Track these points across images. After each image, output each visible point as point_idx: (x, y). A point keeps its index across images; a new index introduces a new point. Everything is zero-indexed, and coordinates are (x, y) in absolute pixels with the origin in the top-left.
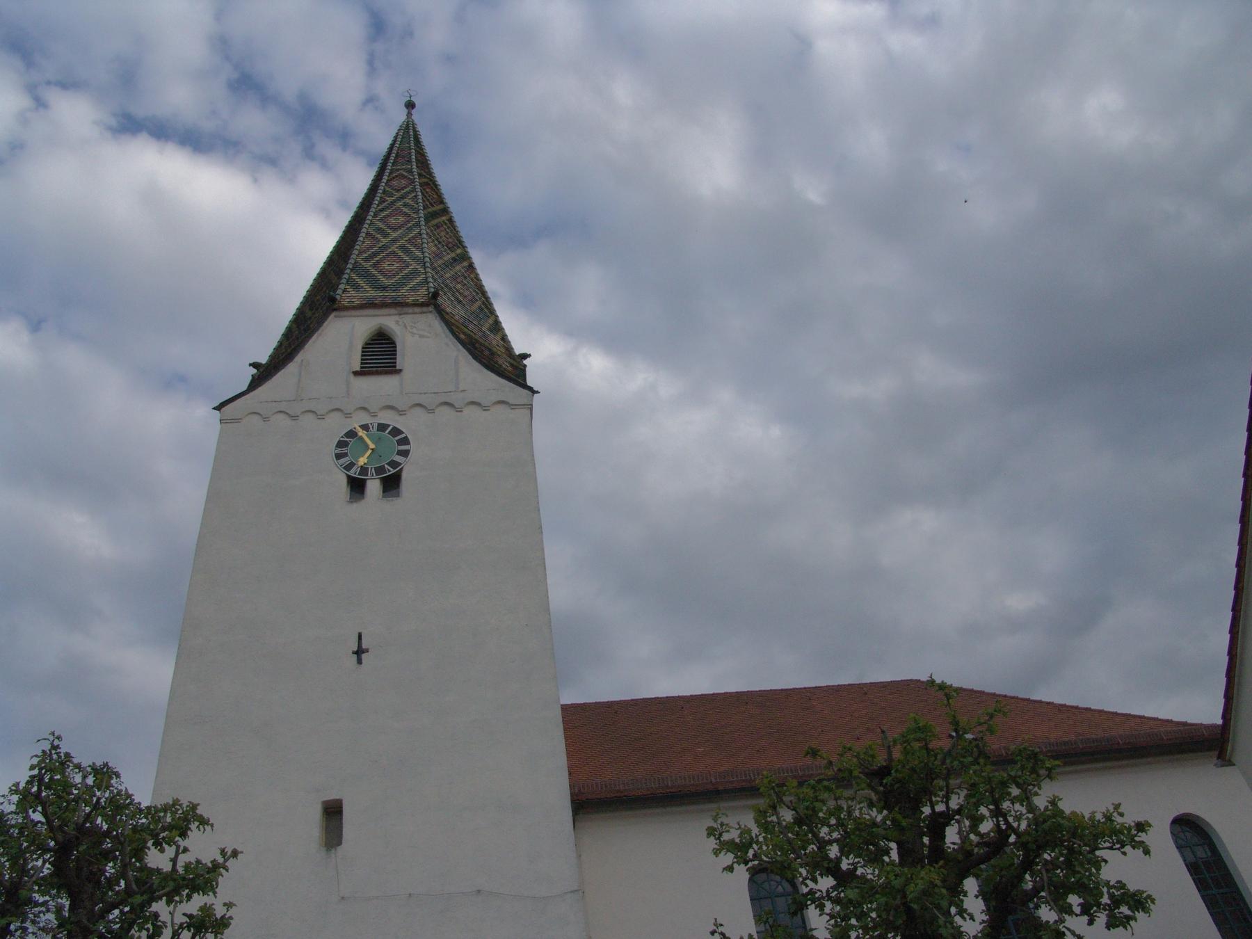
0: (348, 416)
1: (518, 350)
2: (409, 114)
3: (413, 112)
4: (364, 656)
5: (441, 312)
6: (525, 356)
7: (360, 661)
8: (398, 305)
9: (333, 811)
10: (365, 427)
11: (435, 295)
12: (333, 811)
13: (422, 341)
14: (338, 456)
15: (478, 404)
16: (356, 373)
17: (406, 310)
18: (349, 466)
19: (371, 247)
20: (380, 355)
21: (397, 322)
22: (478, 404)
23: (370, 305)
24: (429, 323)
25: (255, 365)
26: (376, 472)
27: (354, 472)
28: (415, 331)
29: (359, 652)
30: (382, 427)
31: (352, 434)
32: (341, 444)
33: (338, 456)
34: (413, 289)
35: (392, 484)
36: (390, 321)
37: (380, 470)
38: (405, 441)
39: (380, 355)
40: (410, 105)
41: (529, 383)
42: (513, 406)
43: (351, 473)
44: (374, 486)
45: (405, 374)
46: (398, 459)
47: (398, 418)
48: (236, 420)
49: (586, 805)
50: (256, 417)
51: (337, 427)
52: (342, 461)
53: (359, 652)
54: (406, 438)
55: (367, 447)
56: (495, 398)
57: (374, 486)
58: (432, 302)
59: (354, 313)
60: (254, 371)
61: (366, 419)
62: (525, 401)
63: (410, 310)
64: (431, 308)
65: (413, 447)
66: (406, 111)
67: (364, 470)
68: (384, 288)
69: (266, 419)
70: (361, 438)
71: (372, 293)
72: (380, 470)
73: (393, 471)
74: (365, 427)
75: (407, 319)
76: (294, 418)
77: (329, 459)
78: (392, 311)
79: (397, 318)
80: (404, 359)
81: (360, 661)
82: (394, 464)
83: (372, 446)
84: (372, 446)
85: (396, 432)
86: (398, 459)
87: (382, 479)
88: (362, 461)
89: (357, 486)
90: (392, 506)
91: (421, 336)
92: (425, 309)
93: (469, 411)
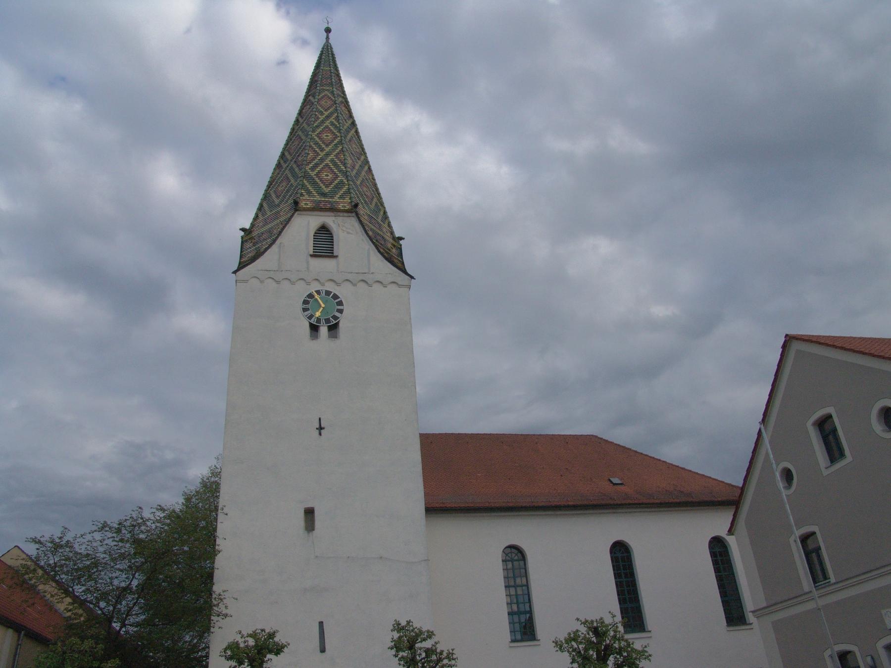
0: (308, 284)
2: (328, 38)
3: (331, 35)
7: (320, 434)
9: (309, 513)
12: (309, 513)
13: (348, 234)
14: (305, 310)
18: (310, 317)
19: (314, 159)
20: (324, 244)
23: (317, 208)
26: (325, 321)
27: (313, 321)
30: (328, 293)
33: (305, 310)
35: (333, 328)
36: (330, 220)
37: (327, 321)
38: (340, 303)
39: (324, 244)
41: (325, 41)
44: (324, 330)
45: (340, 257)
46: (338, 314)
47: (336, 287)
49: (430, 510)
52: (306, 313)
53: (321, 428)
57: (324, 330)
60: (242, 233)
64: (354, 214)
65: (345, 307)
67: (319, 320)
68: (324, 195)
69: (262, 282)
71: (318, 198)
74: (318, 292)
76: (278, 282)
81: (320, 434)
82: (335, 318)
84: (323, 305)
85: (335, 297)
86: (338, 314)
88: (318, 314)
89: (314, 328)
91: (348, 233)
93: (376, 287)
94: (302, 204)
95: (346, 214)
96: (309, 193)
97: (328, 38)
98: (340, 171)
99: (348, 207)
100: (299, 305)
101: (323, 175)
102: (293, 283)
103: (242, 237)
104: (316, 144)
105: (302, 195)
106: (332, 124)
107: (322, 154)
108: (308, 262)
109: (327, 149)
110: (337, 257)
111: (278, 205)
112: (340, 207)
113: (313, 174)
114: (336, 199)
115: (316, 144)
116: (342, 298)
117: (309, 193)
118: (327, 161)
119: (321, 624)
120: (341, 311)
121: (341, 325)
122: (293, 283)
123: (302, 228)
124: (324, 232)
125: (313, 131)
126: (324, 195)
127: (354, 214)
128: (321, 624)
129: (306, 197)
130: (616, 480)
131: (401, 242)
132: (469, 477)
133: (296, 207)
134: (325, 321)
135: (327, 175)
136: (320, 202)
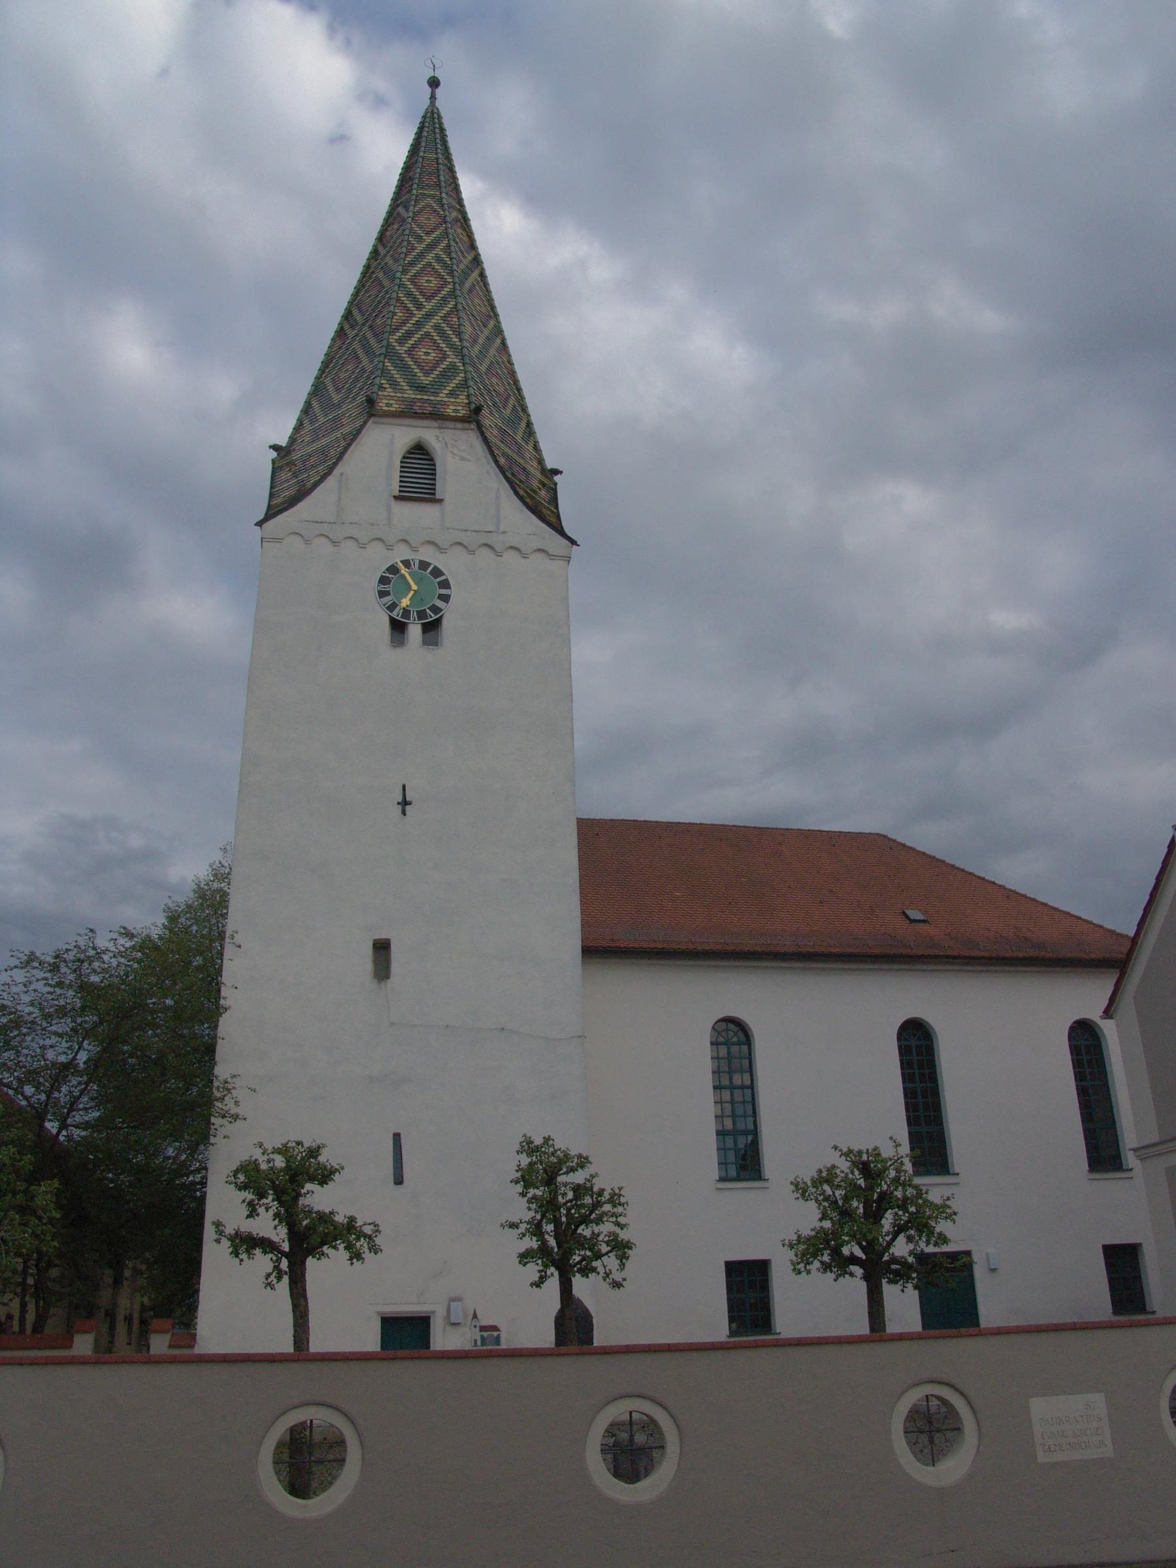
0: (390, 548)
1: (550, 464)
2: (433, 97)
3: (438, 91)
4: (408, 807)
5: (480, 428)
6: (556, 472)
7: (404, 813)
8: (436, 416)
9: (382, 948)
10: (407, 563)
11: (478, 410)
12: (382, 948)
13: (461, 460)
14: (382, 594)
15: (518, 550)
16: (395, 498)
17: (448, 424)
18: (392, 607)
19: (404, 323)
20: (419, 477)
21: (437, 437)
22: (518, 550)
23: (409, 413)
24: (469, 440)
25: (275, 448)
26: (417, 615)
27: (397, 614)
28: (455, 451)
29: (405, 803)
30: (424, 565)
31: (393, 569)
32: (383, 580)
33: (382, 594)
34: (452, 394)
35: (432, 628)
36: (430, 435)
37: (421, 614)
38: (445, 584)
39: (419, 477)
40: (434, 83)
41: (427, 102)
42: (552, 557)
43: (394, 615)
44: (415, 631)
45: (446, 502)
46: (440, 604)
48: (279, 540)
49: (592, 952)
50: (297, 538)
51: (379, 560)
52: (385, 599)
53: (405, 803)
54: (447, 581)
55: (410, 588)
56: (535, 546)
57: (415, 631)
58: (473, 417)
59: (391, 420)
60: (274, 454)
61: (408, 555)
62: (563, 552)
63: (451, 424)
64: (473, 426)
65: (454, 592)
66: (429, 90)
67: (406, 613)
68: (420, 388)
69: (307, 542)
70: (403, 576)
71: (410, 394)
72: (421, 614)
73: (435, 617)
74: (407, 563)
75: (448, 435)
76: (335, 543)
77: (372, 595)
78: (434, 424)
79: (437, 431)
80: (446, 486)
81: (404, 813)
82: (436, 610)
83: (414, 587)
84: (414, 587)
85: (437, 572)
86: (440, 604)
87: (423, 624)
88: (405, 602)
89: (398, 627)
90: (430, 655)
91: (463, 459)
92: (466, 425)
93: (510, 556)
94: (382, 405)
95: (459, 425)
96: (394, 384)
97: (433, 97)
98: (452, 346)
99: (462, 413)
100: (372, 585)
101: (420, 353)
102: (363, 546)
103: (274, 461)
104: (409, 294)
105: (381, 387)
106: (438, 259)
107: (419, 315)
108: (389, 510)
109: (428, 306)
110: (440, 501)
111: (339, 406)
112: (450, 411)
113: (402, 350)
114: (442, 396)
115: (409, 294)
116: (448, 575)
117: (394, 384)
118: (428, 328)
119: (397, 1137)
120: (446, 598)
121: (445, 622)
122: (363, 546)
123: (381, 448)
124: (419, 453)
125: (405, 272)
126: (420, 388)
127: (473, 426)
128: (397, 1137)
129: (389, 391)
130: (914, 914)
131: (556, 478)
132: (668, 897)
133: (371, 410)
134: (417, 615)
135: (427, 354)
136: (413, 401)
